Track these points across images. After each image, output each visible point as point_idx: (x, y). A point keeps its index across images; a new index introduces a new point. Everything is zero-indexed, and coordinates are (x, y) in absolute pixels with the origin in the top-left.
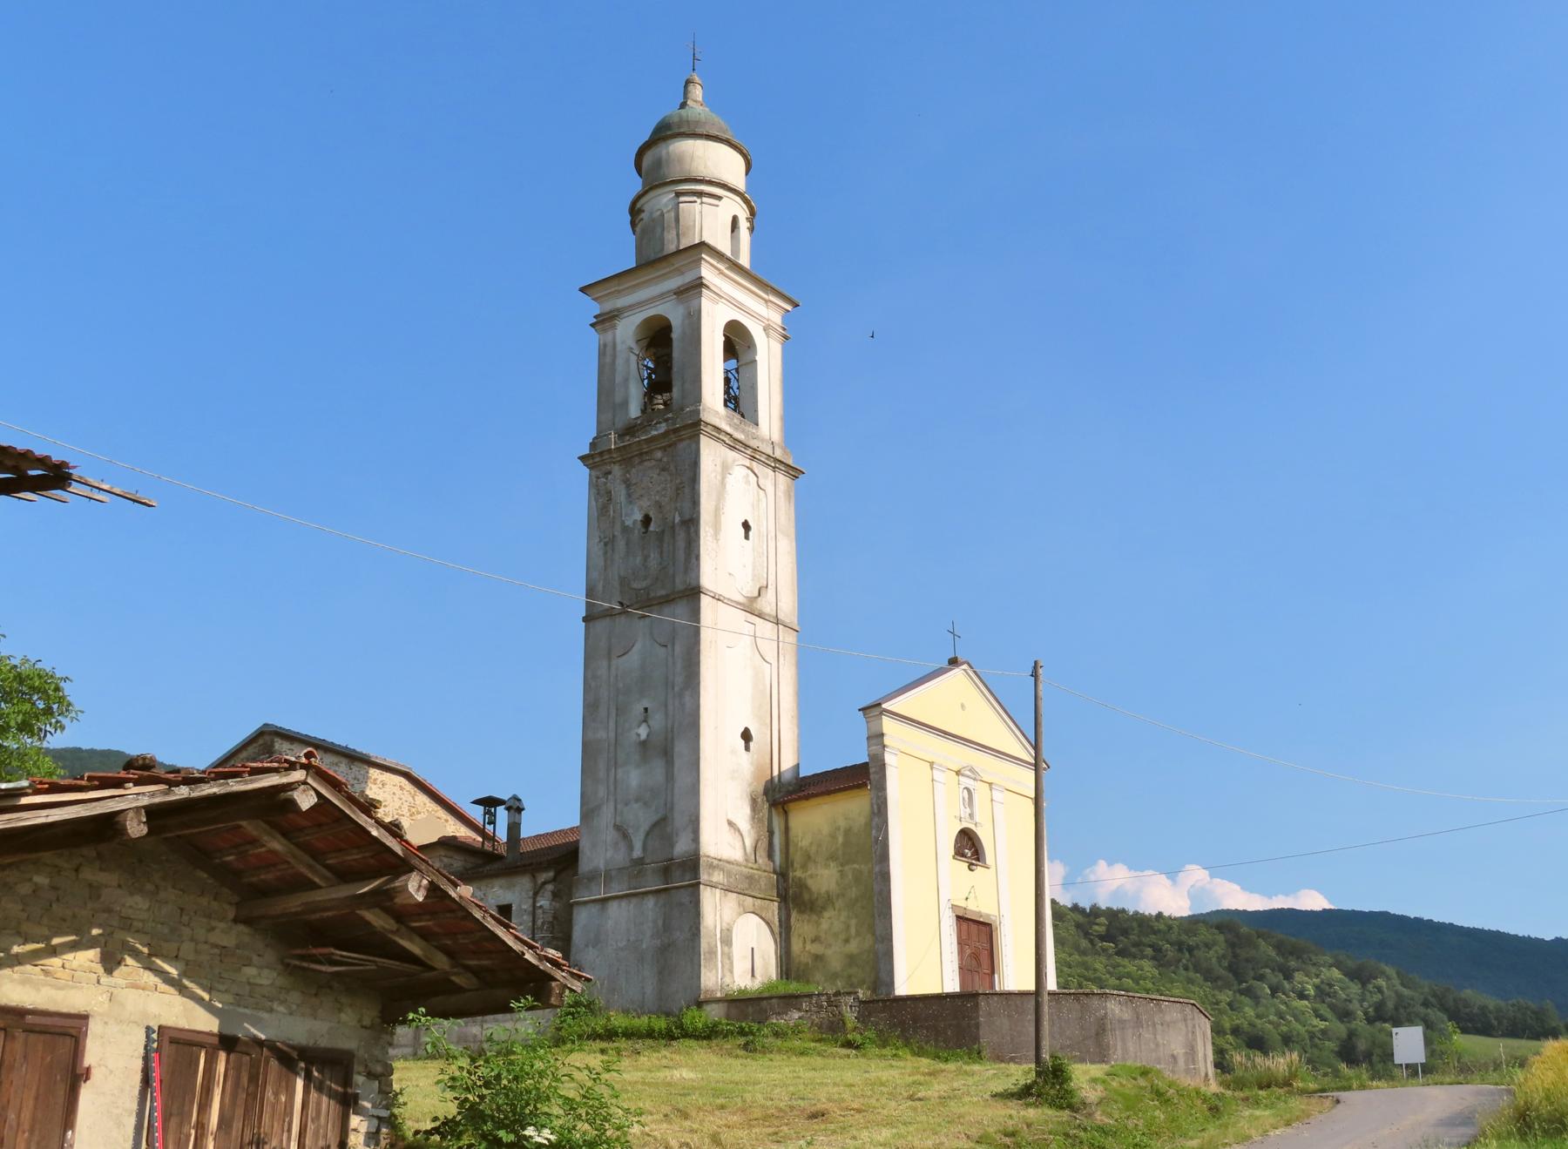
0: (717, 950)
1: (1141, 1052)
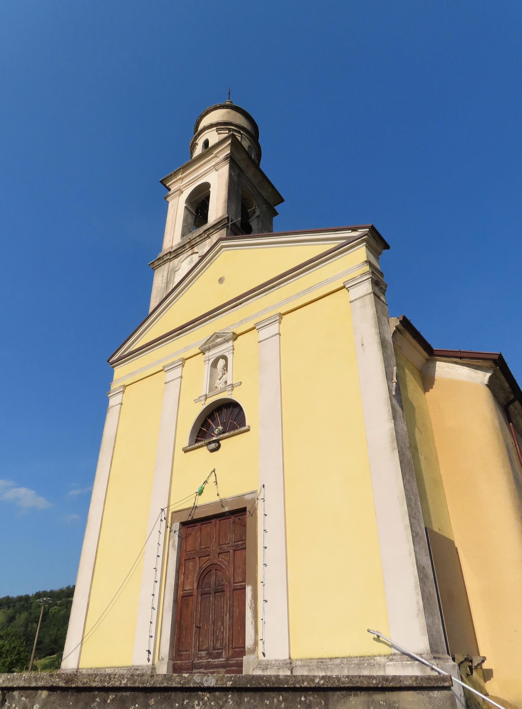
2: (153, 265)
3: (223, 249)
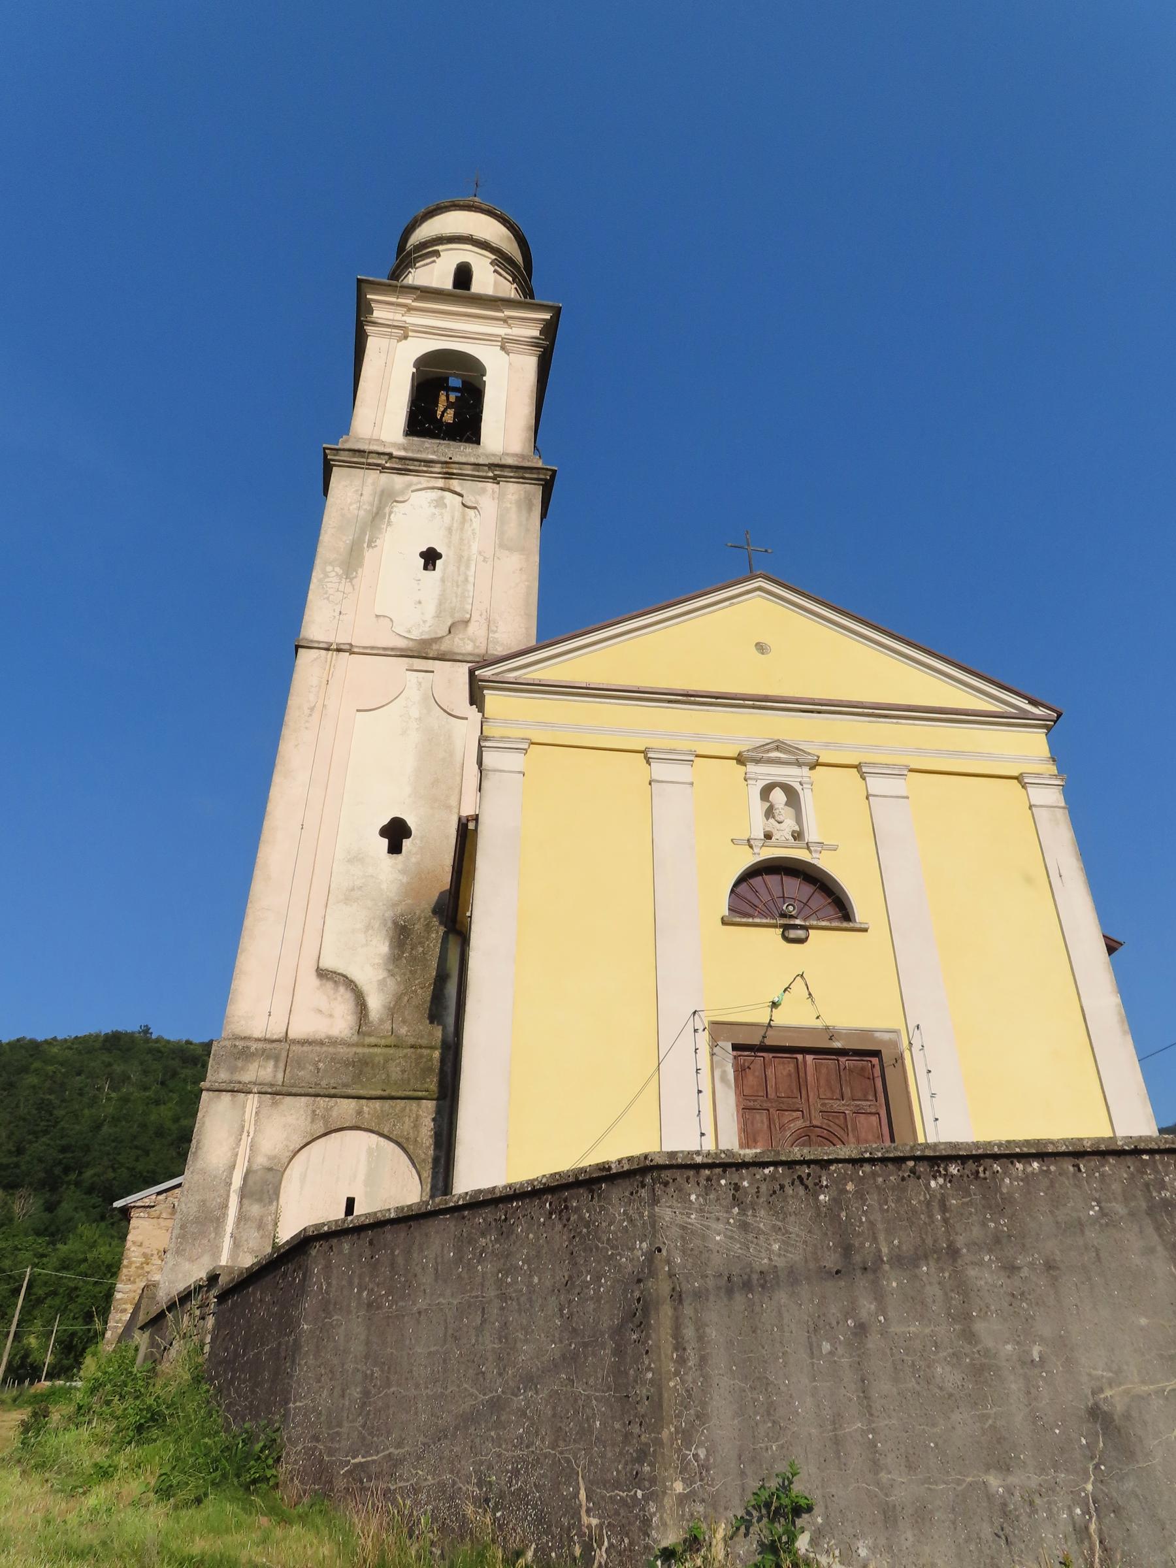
0: (225, 1215)
1: (868, 1411)
2: (335, 455)
3: (758, 593)
